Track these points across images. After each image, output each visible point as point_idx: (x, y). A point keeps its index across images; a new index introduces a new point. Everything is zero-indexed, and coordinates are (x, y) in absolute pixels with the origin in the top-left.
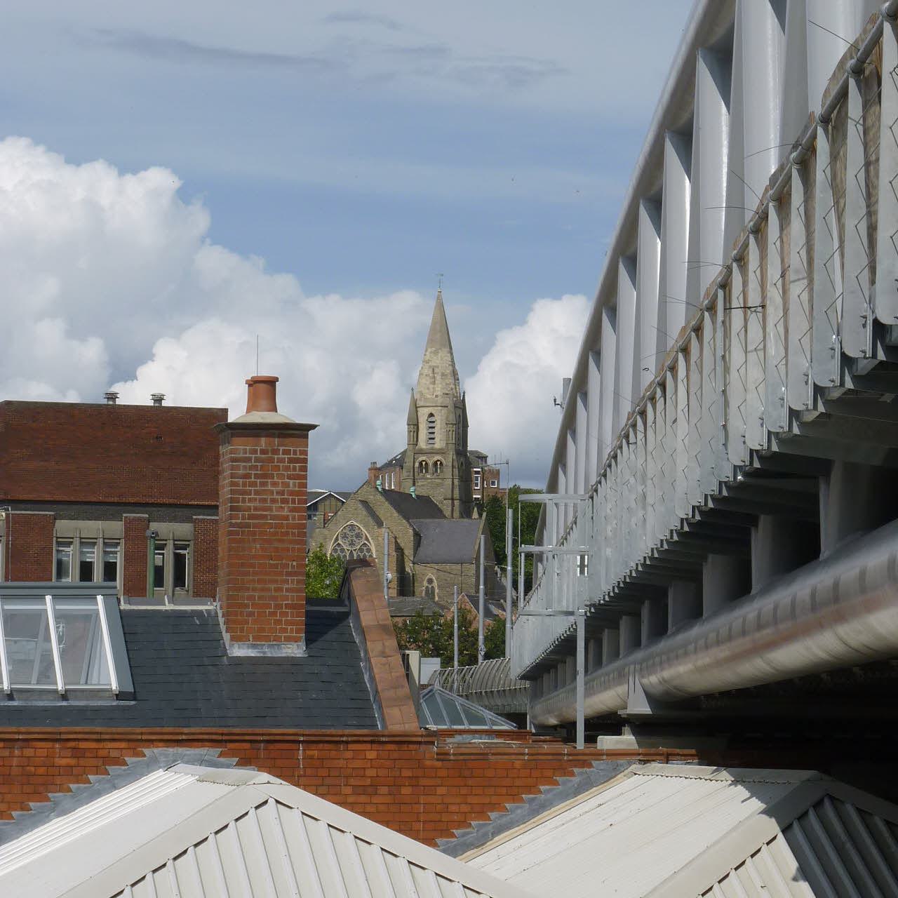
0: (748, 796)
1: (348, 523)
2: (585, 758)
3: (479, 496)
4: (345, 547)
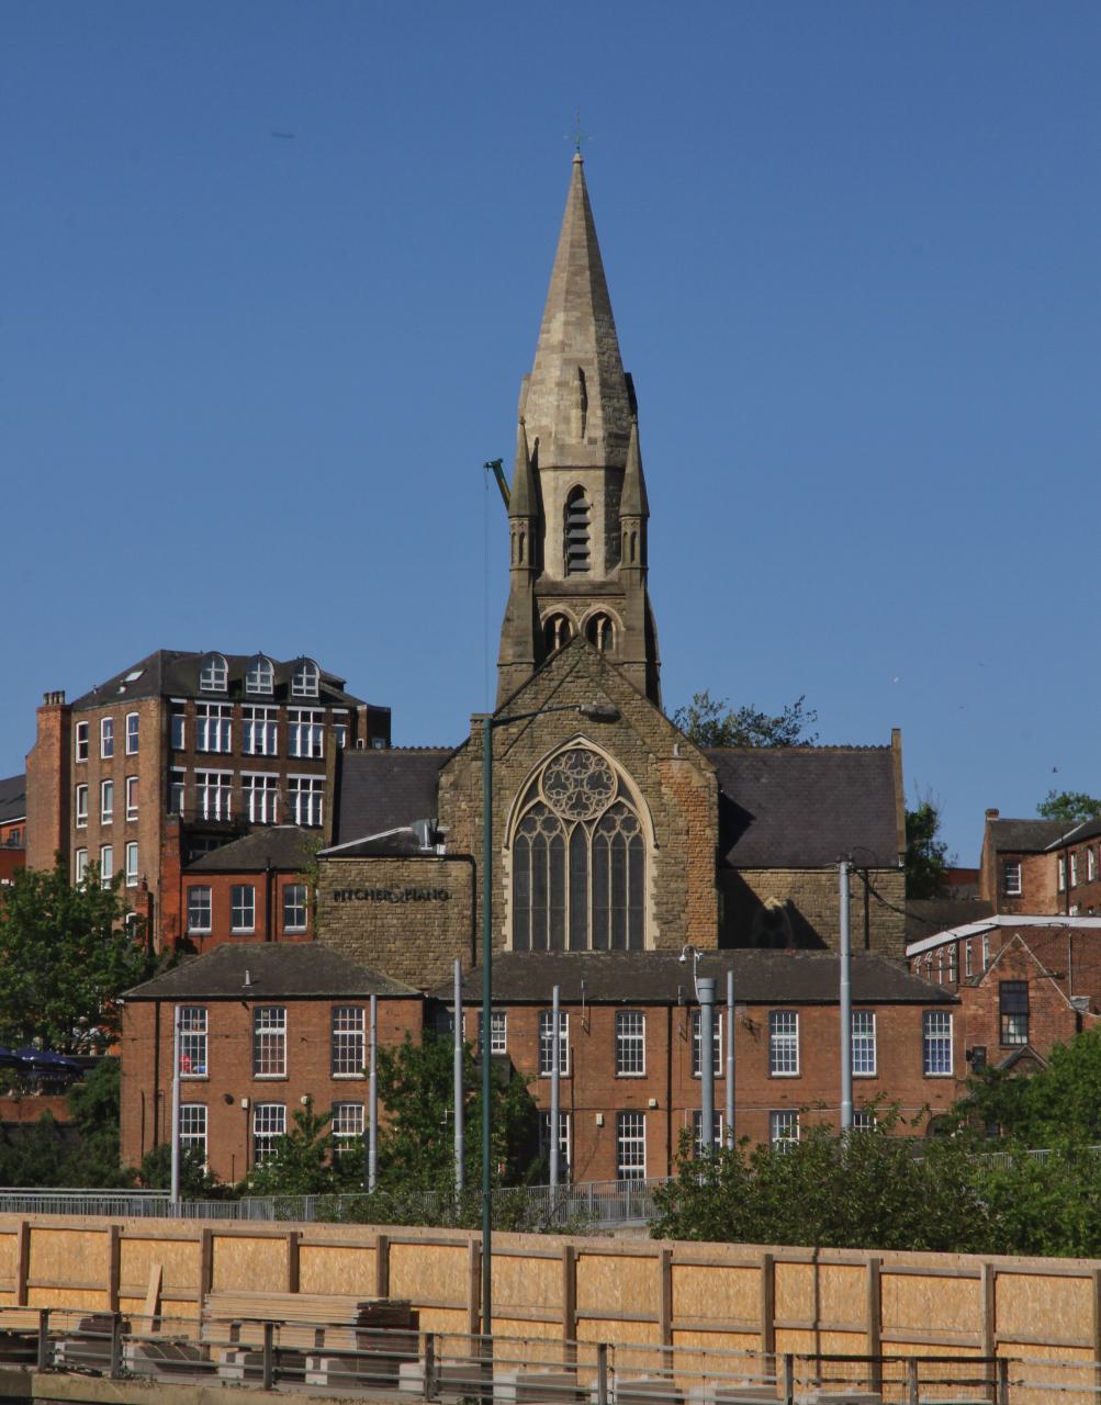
0: (1002, 1275)
1: (569, 746)
2: (676, 1137)
4: (558, 815)
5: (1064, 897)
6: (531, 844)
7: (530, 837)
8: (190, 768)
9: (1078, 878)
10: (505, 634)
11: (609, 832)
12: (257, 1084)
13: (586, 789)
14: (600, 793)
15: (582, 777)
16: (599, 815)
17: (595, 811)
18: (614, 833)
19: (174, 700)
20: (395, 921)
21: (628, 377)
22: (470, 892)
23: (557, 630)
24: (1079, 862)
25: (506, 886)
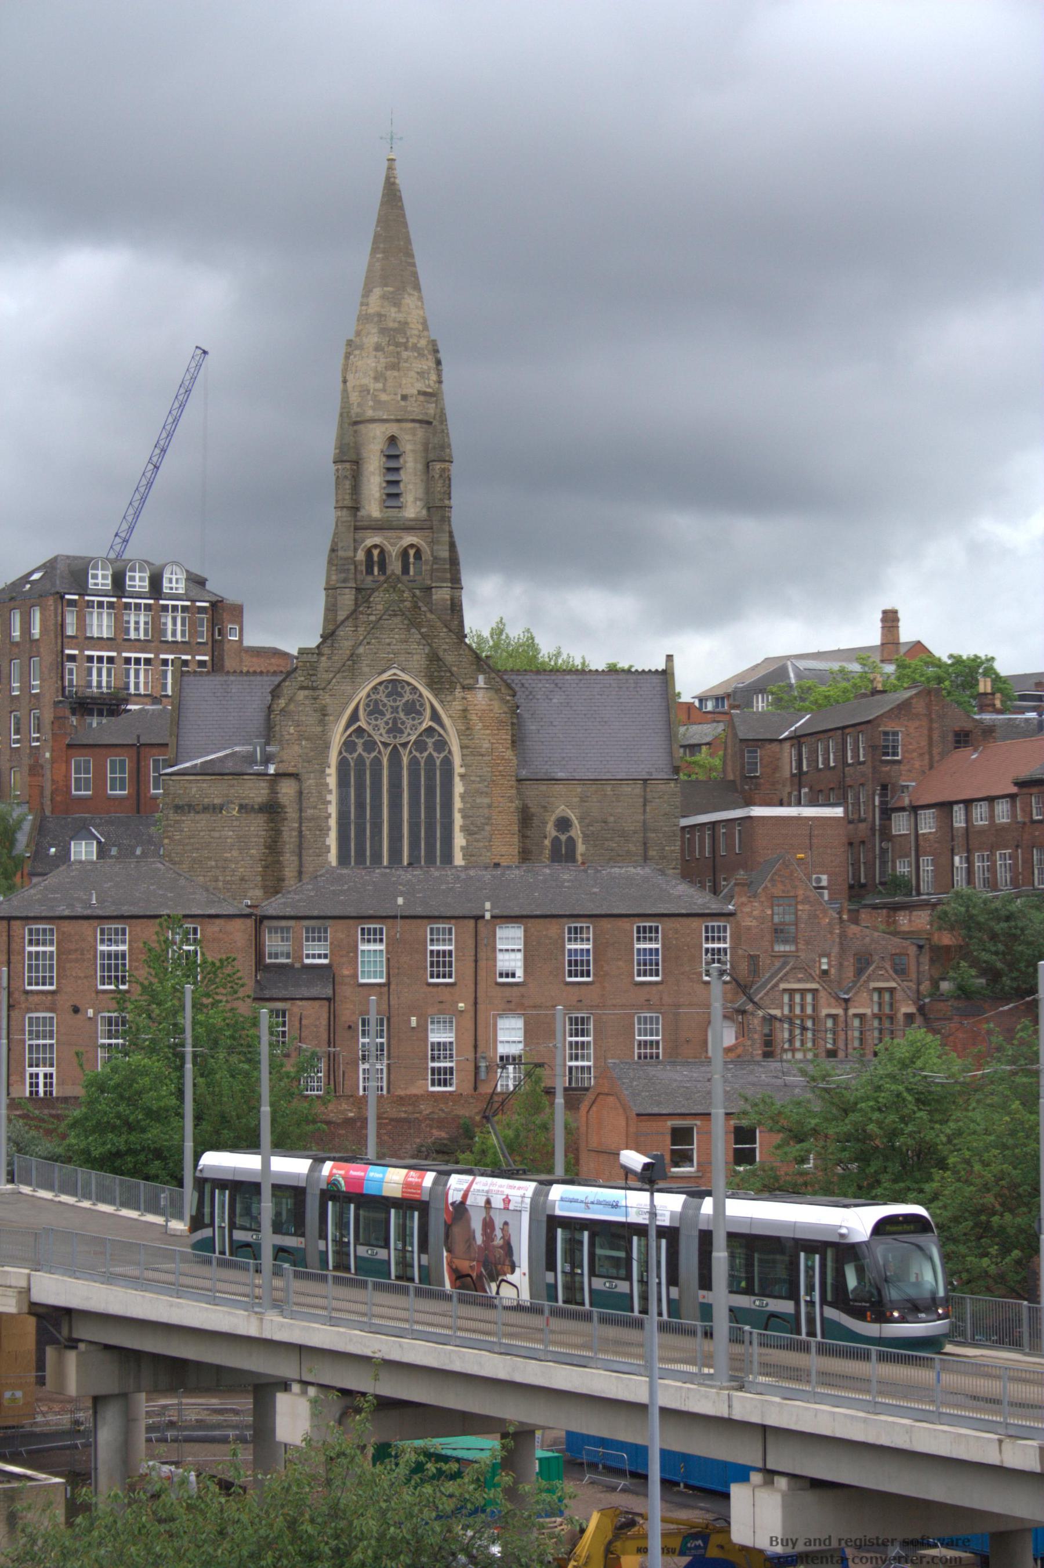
3: (206, 658)
4: (377, 738)
5: (796, 780)
6: (352, 764)
7: (351, 758)
8: (82, 651)
9: (808, 766)
10: (330, 562)
11: (421, 753)
12: (101, 996)
13: (402, 715)
14: (414, 719)
15: (398, 703)
16: (413, 738)
17: (409, 734)
18: (425, 754)
19: (68, 597)
20: (231, 833)
21: (434, 343)
22: (297, 807)
23: (376, 558)
24: (810, 752)
25: (330, 802)
